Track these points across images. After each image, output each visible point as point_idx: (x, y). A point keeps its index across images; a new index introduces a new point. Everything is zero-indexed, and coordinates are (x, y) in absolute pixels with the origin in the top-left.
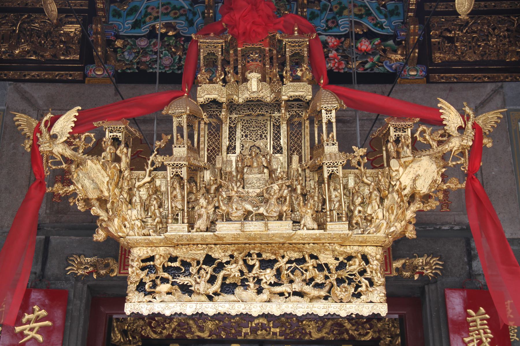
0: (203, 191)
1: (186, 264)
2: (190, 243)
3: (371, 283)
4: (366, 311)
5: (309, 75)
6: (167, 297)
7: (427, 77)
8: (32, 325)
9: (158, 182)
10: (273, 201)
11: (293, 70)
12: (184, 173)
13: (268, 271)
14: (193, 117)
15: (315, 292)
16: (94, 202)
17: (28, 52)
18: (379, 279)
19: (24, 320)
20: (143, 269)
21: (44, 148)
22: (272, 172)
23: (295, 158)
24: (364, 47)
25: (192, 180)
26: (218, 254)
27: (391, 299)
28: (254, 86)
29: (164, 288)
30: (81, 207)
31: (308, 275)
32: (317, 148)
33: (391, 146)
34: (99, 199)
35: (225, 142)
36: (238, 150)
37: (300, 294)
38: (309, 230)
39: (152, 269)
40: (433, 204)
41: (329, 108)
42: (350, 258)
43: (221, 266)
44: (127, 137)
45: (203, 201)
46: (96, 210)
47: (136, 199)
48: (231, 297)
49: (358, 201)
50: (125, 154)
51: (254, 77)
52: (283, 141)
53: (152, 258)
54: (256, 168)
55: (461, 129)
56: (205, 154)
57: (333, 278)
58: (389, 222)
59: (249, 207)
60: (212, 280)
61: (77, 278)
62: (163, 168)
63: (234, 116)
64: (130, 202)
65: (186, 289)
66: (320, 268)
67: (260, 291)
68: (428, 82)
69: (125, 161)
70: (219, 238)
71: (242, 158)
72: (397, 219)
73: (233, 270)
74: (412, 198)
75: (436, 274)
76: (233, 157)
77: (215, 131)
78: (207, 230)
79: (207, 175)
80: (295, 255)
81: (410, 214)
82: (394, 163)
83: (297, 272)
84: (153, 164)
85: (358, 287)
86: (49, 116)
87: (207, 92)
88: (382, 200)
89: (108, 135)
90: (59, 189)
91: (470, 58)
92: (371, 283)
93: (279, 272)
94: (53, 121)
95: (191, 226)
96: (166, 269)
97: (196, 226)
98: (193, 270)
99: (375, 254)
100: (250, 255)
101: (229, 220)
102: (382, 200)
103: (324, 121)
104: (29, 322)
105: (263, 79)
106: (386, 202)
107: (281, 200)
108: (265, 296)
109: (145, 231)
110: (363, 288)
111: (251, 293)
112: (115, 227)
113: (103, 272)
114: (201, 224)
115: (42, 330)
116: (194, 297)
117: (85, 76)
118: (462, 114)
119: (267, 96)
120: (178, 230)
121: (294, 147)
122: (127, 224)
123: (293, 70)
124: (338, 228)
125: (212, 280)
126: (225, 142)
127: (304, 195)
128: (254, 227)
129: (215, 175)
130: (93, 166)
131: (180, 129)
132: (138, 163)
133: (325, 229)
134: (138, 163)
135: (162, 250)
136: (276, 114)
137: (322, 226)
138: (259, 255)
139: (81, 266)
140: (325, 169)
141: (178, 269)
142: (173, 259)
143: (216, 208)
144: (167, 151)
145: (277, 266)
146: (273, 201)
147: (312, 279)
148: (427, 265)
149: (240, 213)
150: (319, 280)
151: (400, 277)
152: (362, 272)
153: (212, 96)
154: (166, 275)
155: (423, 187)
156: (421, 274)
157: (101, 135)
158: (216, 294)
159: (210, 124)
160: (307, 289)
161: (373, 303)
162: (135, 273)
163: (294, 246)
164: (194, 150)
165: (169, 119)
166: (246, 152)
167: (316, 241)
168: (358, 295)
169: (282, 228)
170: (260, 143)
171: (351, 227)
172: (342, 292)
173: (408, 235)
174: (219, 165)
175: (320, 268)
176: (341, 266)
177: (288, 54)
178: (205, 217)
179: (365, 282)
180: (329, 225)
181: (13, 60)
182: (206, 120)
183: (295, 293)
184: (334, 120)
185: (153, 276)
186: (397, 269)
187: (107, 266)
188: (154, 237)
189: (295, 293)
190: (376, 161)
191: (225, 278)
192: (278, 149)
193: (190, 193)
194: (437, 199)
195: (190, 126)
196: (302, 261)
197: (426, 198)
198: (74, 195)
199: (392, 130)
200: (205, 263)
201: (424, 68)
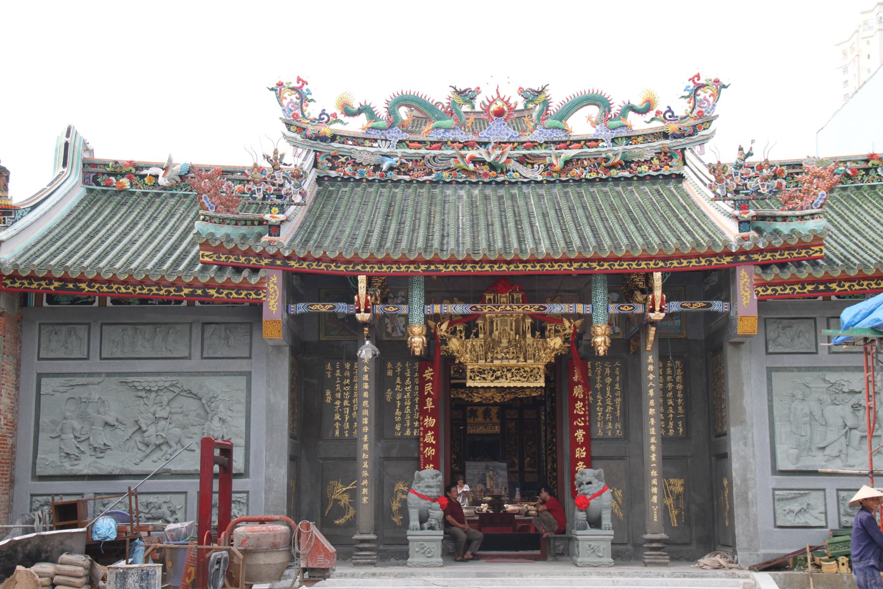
4: (538, 385)
21: (439, 333)
27: (546, 382)
58: (546, 357)
65: (484, 378)
71: (500, 333)
99: (542, 367)
111: (504, 380)
112: (462, 360)
115: (432, 376)
118: (570, 322)
120: (481, 362)
130: (454, 340)
132: (467, 337)
134: (467, 337)
137: (526, 361)
155: (557, 347)
157: (455, 328)
161: (541, 383)
162: (469, 374)
164: (485, 333)
169: (513, 362)
176: (532, 371)
190: (543, 336)
192: (511, 330)
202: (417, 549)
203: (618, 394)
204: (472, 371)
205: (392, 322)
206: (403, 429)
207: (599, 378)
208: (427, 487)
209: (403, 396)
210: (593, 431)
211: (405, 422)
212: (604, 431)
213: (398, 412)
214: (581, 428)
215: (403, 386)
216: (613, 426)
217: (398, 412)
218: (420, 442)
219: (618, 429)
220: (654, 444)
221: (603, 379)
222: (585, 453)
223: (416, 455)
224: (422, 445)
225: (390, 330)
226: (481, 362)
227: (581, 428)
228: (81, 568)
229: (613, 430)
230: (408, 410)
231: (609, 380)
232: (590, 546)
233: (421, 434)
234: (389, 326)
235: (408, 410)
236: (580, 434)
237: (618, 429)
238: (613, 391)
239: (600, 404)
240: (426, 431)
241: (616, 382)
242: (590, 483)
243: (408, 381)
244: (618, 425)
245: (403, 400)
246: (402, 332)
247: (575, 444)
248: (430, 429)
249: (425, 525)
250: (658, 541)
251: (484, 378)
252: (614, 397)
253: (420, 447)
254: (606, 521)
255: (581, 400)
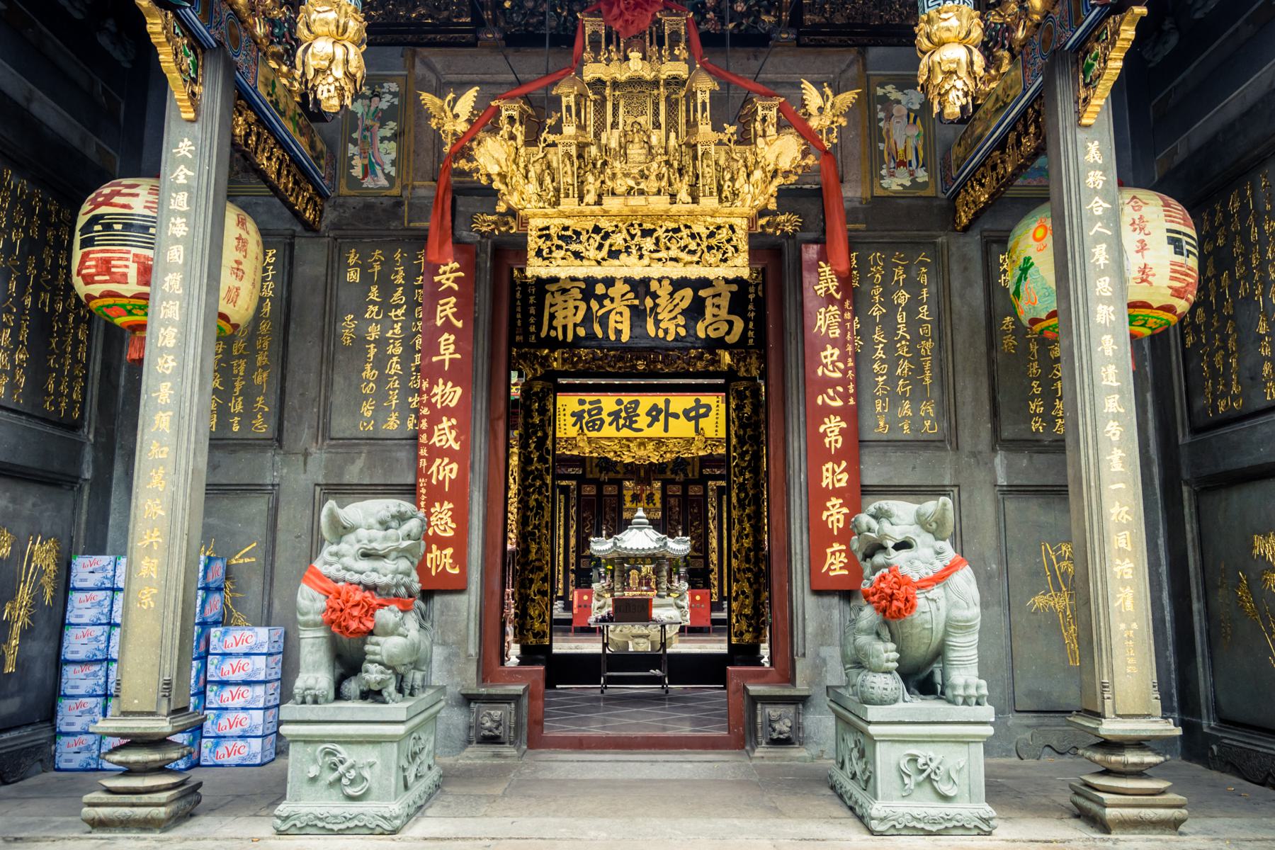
0: (590, 166)
1: (578, 233)
2: (581, 215)
3: (737, 250)
5: (685, 54)
6: (560, 262)
7: (797, 39)
8: (448, 275)
9: (549, 156)
10: (653, 177)
11: (671, 48)
12: (573, 151)
13: (649, 239)
14: (581, 96)
15: (688, 258)
16: (494, 177)
17: (423, 15)
18: (744, 246)
19: (441, 271)
20: (540, 237)
22: (651, 148)
23: (673, 135)
24: (739, 9)
25: (580, 156)
26: (605, 224)
28: (636, 65)
29: (558, 254)
30: (484, 181)
31: (682, 243)
32: (692, 125)
33: (758, 126)
34: (499, 174)
35: (609, 119)
36: (621, 126)
37: (676, 260)
38: (683, 206)
39: (548, 237)
40: (793, 178)
41: (705, 87)
42: (719, 228)
43: (607, 236)
44: (521, 115)
45: (590, 178)
46: (497, 185)
47: (532, 174)
48: (616, 262)
49: (728, 176)
50: (519, 130)
51: (635, 56)
52: (662, 118)
53: (547, 228)
54: (638, 141)
55: (821, 110)
56: (591, 129)
57: (704, 246)
58: (755, 194)
59: (632, 183)
60: (600, 247)
61: (482, 234)
62: (554, 145)
63: (617, 93)
64: (527, 177)
65: (577, 255)
66: (693, 236)
67: (641, 257)
68: (799, 45)
69: (520, 138)
70: (605, 212)
72: (762, 193)
73: (618, 240)
74: (775, 173)
75: (795, 230)
76: (616, 133)
77: (600, 105)
78: (595, 204)
79: (594, 150)
80: (672, 225)
81: (772, 189)
82: (760, 141)
83: (674, 241)
84: (545, 140)
85: (725, 253)
86: (451, 96)
87: (592, 71)
88: (748, 176)
89: (504, 113)
90: (463, 164)
91: (839, 20)
92: (737, 250)
93: (657, 239)
94: (455, 100)
95: (581, 199)
96: (560, 237)
97: (586, 200)
98: (584, 237)
99: (741, 224)
100: (632, 225)
101: (614, 194)
102: (748, 176)
103: (699, 101)
104: (444, 273)
105: (644, 59)
106: (752, 179)
107: (660, 177)
108: (646, 261)
109: (541, 204)
110: (730, 254)
111: (634, 258)
112: (514, 200)
113: (503, 229)
114: (591, 198)
115: (456, 280)
116: (585, 262)
117: (477, 39)
118: (822, 94)
119: (649, 75)
121: (672, 125)
122: (523, 196)
123: (671, 48)
124: (709, 203)
125: (600, 247)
126: (609, 119)
127: (680, 170)
128: (637, 201)
129: (601, 151)
131: (569, 108)
133: (698, 203)
134: (531, 141)
135: (558, 221)
136: (656, 92)
137: (695, 200)
138: (640, 225)
139: (485, 222)
140: (699, 147)
141: (571, 237)
142: (566, 228)
143: (603, 182)
144: (557, 129)
145: (655, 235)
146: (653, 177)
147: (686, 247)
148: (788, 222)
149: (623, 189)
150: (693, 246)
151: (763, 234)
152: (729, 241)
153: (598, 75)
154: (560, 243)
155: (785, 164)
156: (782, 230)
158: (603, 259)
159: (595, 101)
160: (684, 256)
162: (533, 242)
163: (669, 217)
164: (582, 127)
165: (558, 99)
166: (628, 128)
167: (691, 214)
168: (725, 260)
169: (660, 203)
170: (641, 120)
171: (721, 201)
172: (710, 258)
173: (770, 207)
174: (604, 141)
175: (693, 236)
176: (712, 235)
177: (667, 32)
178: (593, 192)
179: (731, 249)
180: (702, 200)
181: (410, 22)
182: (592, 97)
183: (671, 259)
184: (707, 101)
185: (549, 243)
186: (762, 226)
187: (506, 223)
188: (550, 211)
189: (671, 259)
190: (745, 138)
191: (611, 246)
192: (657, 125)
193: (579, 168)
194: (796, 174)
195: (578, 104)
196: (677, 230)
197: (787, 174)
198: (477, 170)
199: (760, 108)
200: (593, 232)
201: (795, 31)
202: (313, 771)
203: (926, 330)
204: (545, 234)
205: (363, 154)
206: (381, 411)
207: (877, 291)
208: (366, 555)
209: (384, 331)
210: (866, 421)
211: (386, 397)
212: (893, 424)
213: (369, 372)
214: (835, 411)
215: (385, 306)
216: (916, 410)
217: (369, 372)
218: (417, 446)
219: (927, 416)
220: (1116, 416)
221: (887, 294)
222: (845, 476)
223: (410, 479)
224: (423, 452)
225: (357, 172)
226: (569, 204)
227: (835, 411)
228: (260, 662)
229: (916, 421)
230: (394, 367)
231: (902, 297)
232: (914, 759)
233: (424, 425)
234: (357, 162)
235: (394, 367)
236: (833, 429)
237: (927, 416)
238: (913, 324)
239: (880, 354)
240: (436, 415)
241: (921, 303)
242: (903, 545)
243: (398, 296)
244: (928, 409)
245: (382, 342)
246: (388, 176)
247: (818, 453)
248: (448, 412)
249: (352, 686)
250: (1139, 744)
251: (577, 255)
252: (916, 339)
253: (417, 457)
254: (964, 673)
255: (834, 343)
